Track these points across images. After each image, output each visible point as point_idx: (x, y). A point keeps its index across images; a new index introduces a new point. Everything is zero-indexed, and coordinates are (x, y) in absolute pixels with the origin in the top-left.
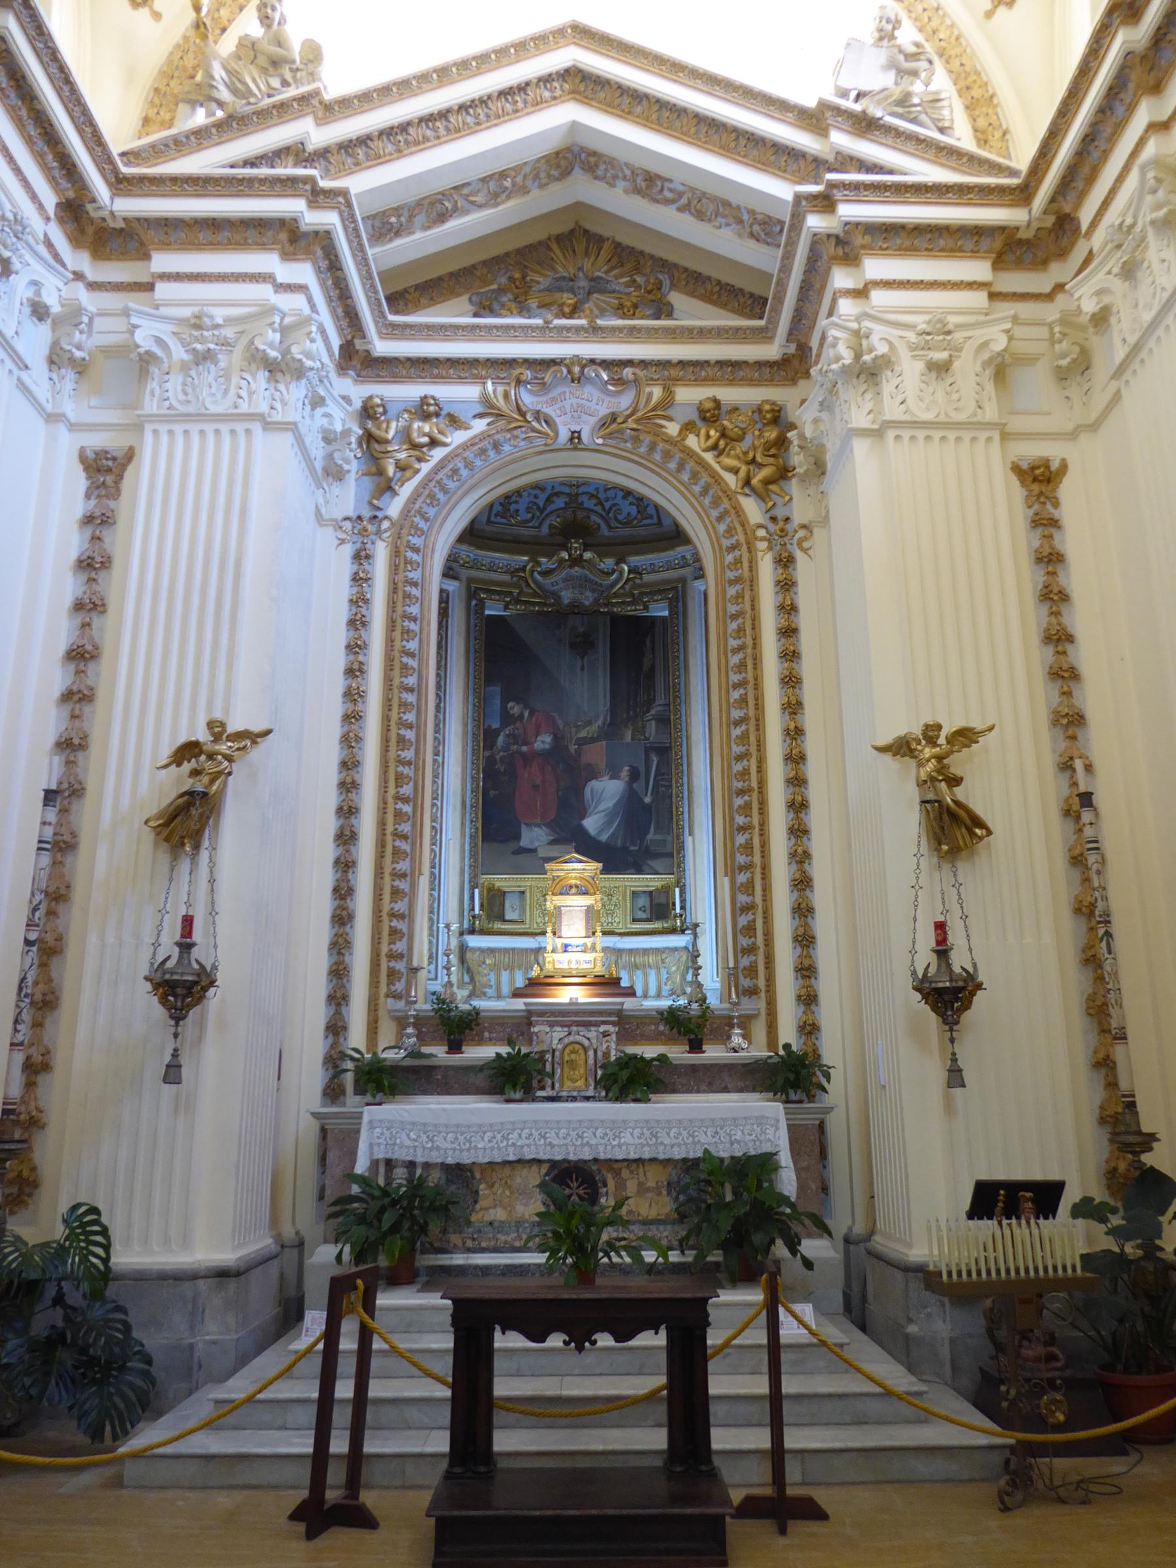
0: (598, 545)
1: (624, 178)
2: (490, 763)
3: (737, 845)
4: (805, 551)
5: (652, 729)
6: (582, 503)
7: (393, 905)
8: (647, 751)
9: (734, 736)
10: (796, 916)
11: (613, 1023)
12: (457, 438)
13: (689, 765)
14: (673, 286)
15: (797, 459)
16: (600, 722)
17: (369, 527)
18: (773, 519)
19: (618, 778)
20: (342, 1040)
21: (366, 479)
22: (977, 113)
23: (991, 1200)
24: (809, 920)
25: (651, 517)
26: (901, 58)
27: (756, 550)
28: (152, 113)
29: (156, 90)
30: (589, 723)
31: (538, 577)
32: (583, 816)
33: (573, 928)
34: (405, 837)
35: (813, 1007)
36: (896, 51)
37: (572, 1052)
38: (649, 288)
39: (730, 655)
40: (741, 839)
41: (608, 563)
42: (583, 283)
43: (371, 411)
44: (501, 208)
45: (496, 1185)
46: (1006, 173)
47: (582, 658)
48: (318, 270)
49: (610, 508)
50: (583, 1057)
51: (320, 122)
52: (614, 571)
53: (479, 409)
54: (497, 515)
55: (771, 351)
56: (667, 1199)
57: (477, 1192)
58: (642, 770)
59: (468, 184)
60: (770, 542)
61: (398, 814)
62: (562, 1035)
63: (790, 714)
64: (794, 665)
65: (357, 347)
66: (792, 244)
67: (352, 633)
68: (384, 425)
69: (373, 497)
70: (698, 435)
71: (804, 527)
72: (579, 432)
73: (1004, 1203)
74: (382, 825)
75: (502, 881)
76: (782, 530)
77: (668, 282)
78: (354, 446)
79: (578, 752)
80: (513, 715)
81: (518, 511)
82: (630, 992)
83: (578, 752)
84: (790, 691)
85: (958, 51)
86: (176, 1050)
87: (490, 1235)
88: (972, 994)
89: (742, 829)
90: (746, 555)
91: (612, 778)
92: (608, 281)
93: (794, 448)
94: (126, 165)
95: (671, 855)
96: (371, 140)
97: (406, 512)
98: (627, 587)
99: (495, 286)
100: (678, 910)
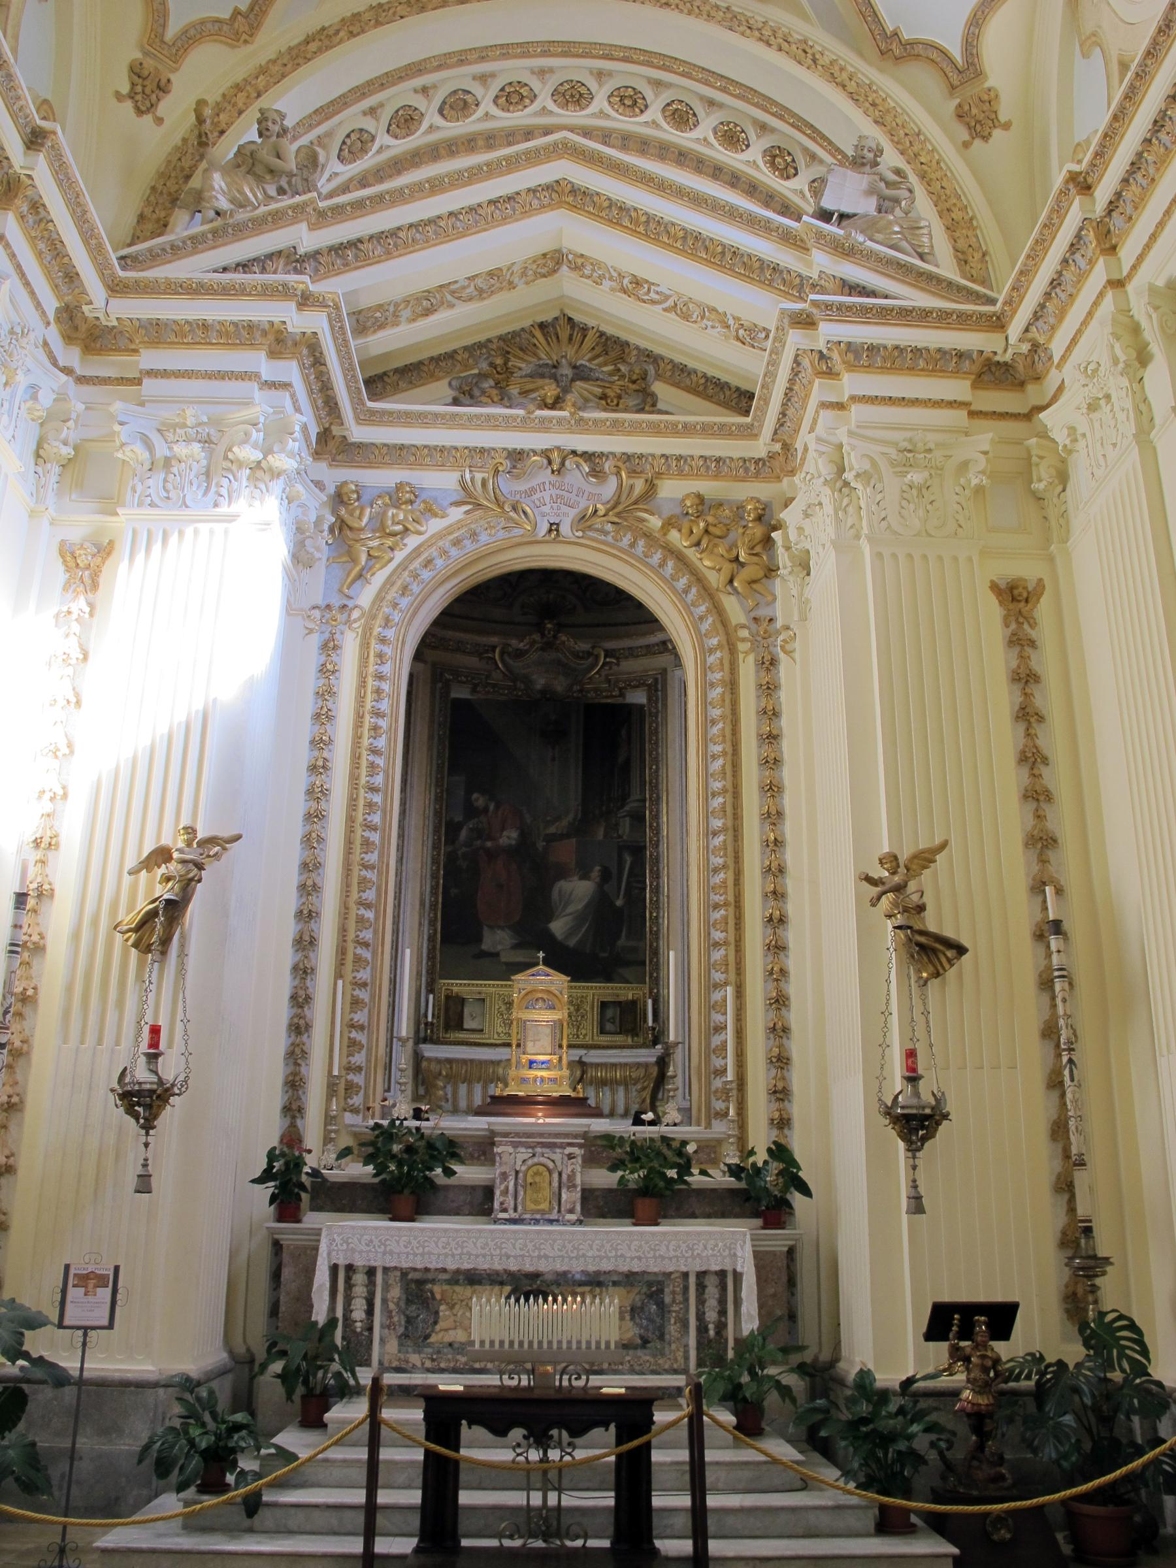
1: (611, 278)
2: (451, 858)
5: (625, 827)
7: (352, 1015)
11: (580, 1146)
12: (434, 526)
14: (658, 376)
15: (783, 557)
16: (571, 817)
17: (339, 616)
22: (957, 234)
23: (944, 1321)
26: (883, 185)
28: (148, 211)
29: (153, 188)
33: (540, 1047)
34: (366, 945)
35: (786, 1131)
36: (877, 178)
37: (537, 1173)
38: (635, 377)
42: (566, 371)
43: (345, 499)
44: (486, 302)
45: (457, 1307)
46: (983, 300)
48: (302, 366)
51: (312, 227)
53: (455, 497)
55: (760, 447)
56: (631, 1324)
57: (437, 1313)
58: (614, 871)
59: (456, 282)
61: (361, 920)
62: (526, 1156)
65: (334, 433)
66: (776, 352)
67: (317, 727)
68: (358, 512)
70: (680, 531)
72: (558, 524)
73: (958, 1326)
74: (343, 930)
75: (459, 986)
77: (653, 372)
78: (326, 533)
85: (939, 174)
86: (146, 1160)
87: (450, 1356)
88: (938, 1124)
91: (581, 878)
92: (591, 370)
93: (780, 551)
94: (123, 268)
96: (362, 242)
99: (476, 371)
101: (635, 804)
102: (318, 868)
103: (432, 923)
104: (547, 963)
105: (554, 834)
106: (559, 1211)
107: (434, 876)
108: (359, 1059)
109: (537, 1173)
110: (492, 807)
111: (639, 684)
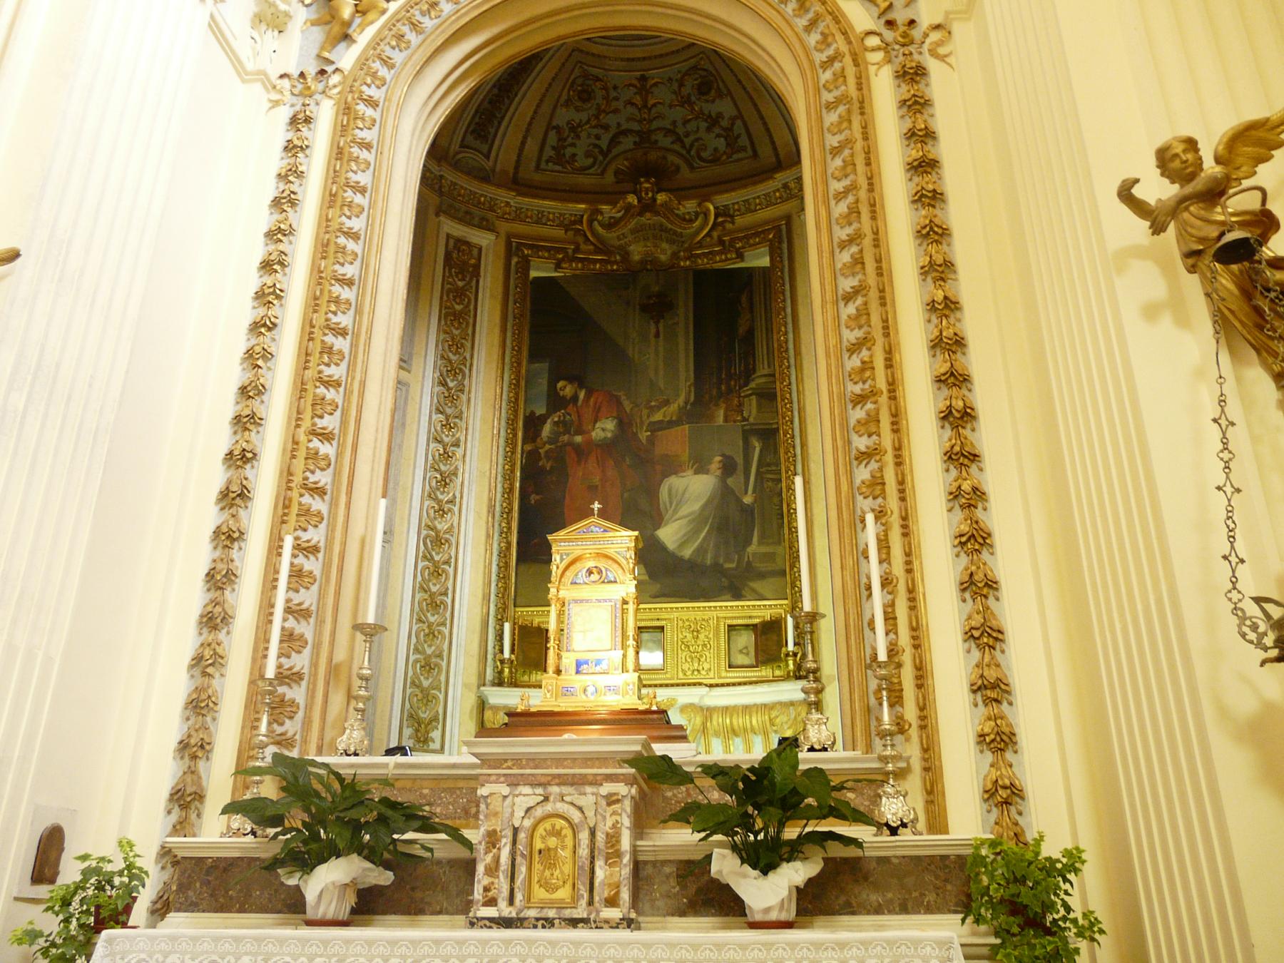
0: (678, 189)
3: (858, 482)
4: (942, 58)
6: (656, 141)
8: (746, 435)
9: (844, 317)
10: (967, 595)
13: (804, 445)
16: (681, 400)
18: (890, 24)
19: (707, 472)
20: (193, 816)
21: (315, 29)
24: (991, 601)
25: (743, 149)
27: (867, 63)
30: (667, 403)
31: (600, 230)
32: (658, 526)
35: (1009, 755)
39: (833, 202)
40: (863, 474)
41: (690, 206)
47: (657, 323)
49: (692, 145)
50: (569, 842)
52: (697, 214)
54: (547, 162)
60: (887, 52)
63: (935, 280)
64: (937, 211)
69: (322, 48)
71: (937, 27)
76: (905, 35)
79: (651, 440)
80: (564, 397)
81: (574, 155)
82: (679, 735)
83: (651, 440)
84: (933, 249)
89: (865, 456)
90: (851, 71)
91: (696, 472)
95: (783, 573)
97: (362, 63)
98: (715, 234)
100: (791, 647)
101: (763, 380)
102: (260, 393)
103: (504, 534)
104: (603, 514)
105: (661, 422)
106: (591, 903)
107: (508, 477)
108: (300, 661)
109: (557, 833)
110: (582, 395)
111: (754, 235)
